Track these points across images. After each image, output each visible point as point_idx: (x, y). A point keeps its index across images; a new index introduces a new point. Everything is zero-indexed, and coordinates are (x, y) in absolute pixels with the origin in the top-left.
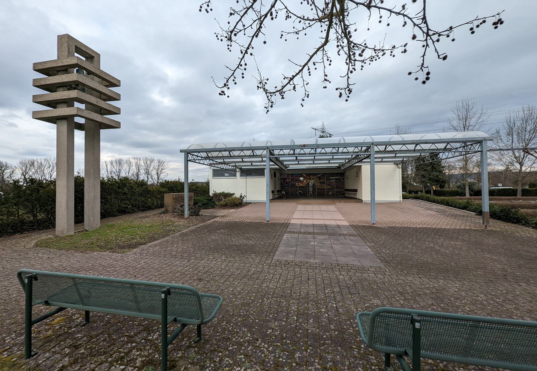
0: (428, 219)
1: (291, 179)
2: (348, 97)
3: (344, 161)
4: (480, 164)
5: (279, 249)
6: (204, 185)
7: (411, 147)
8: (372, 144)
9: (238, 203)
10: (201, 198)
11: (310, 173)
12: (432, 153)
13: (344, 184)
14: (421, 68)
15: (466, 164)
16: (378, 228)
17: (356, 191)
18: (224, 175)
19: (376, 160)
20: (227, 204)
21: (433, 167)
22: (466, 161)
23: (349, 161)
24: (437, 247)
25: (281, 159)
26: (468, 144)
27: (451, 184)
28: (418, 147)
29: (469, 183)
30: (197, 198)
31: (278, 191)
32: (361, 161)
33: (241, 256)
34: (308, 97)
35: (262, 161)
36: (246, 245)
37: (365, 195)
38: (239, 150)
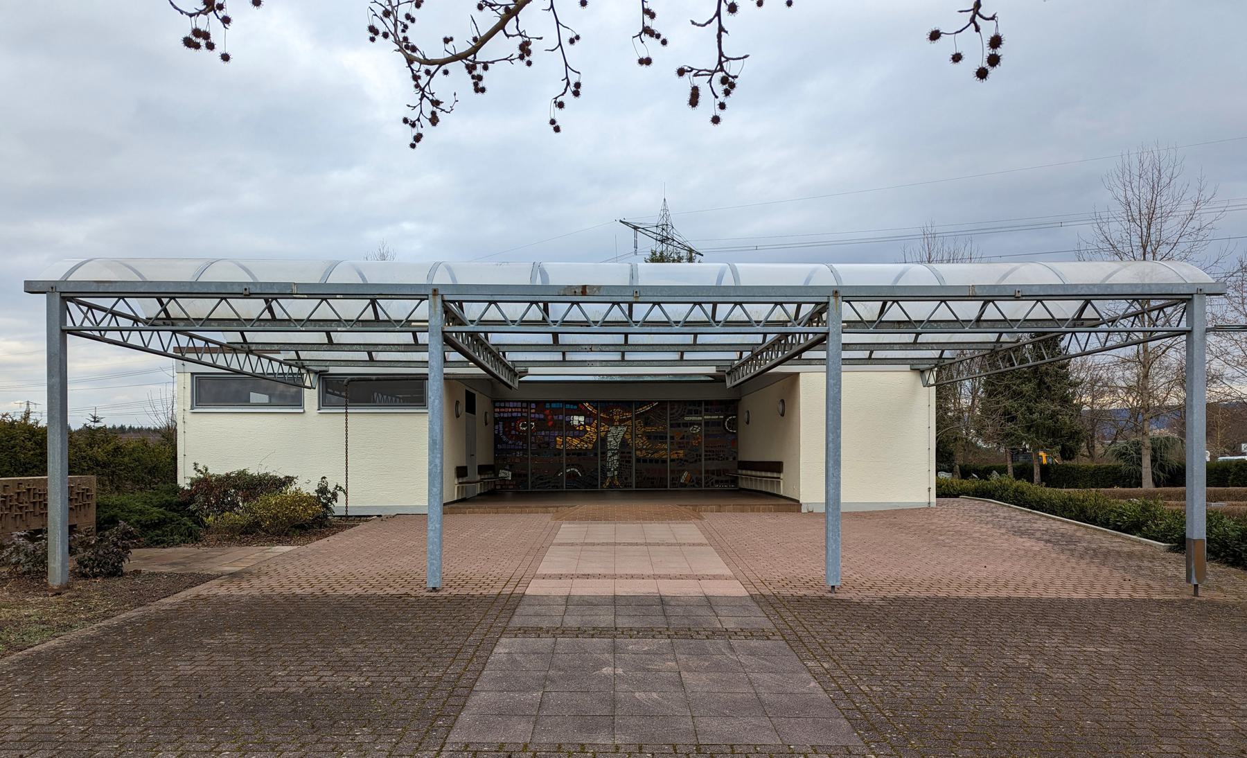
0: (1016, 569)
1: (538, 421)
2: (722, 106)
3: (735, 356)
4: (1184, 378)
5: (474, 700)
6: (153, 441)
7: (968, 310)
8: (836, 294)
9: (313, 519)
10: (134, 499)
11: (610, 400)
12: (1038, 334)
13: (735, 441)
14: (973, 20)
15: (1146, 376)
16: (846, 604)
17: (777, 467)
18: (245, 402)
19: (845, 355)
20: (258, 524)
21: (1041, 383)
22: (1145, 363)
23: (754, 356)
24: (1040, 667)
25: (494, 339)
26: (1153, 303)
27: (1098, 446)
28: (991, 313)
29: (1153, 440)
30: (114, 498)
31: (482, 469)
32: (796, 356)
33: (309, 738)
34: (576, 94)
35: (417, 346)
36: (336, 692)
37: (808, 485)
38: (311, 296)
